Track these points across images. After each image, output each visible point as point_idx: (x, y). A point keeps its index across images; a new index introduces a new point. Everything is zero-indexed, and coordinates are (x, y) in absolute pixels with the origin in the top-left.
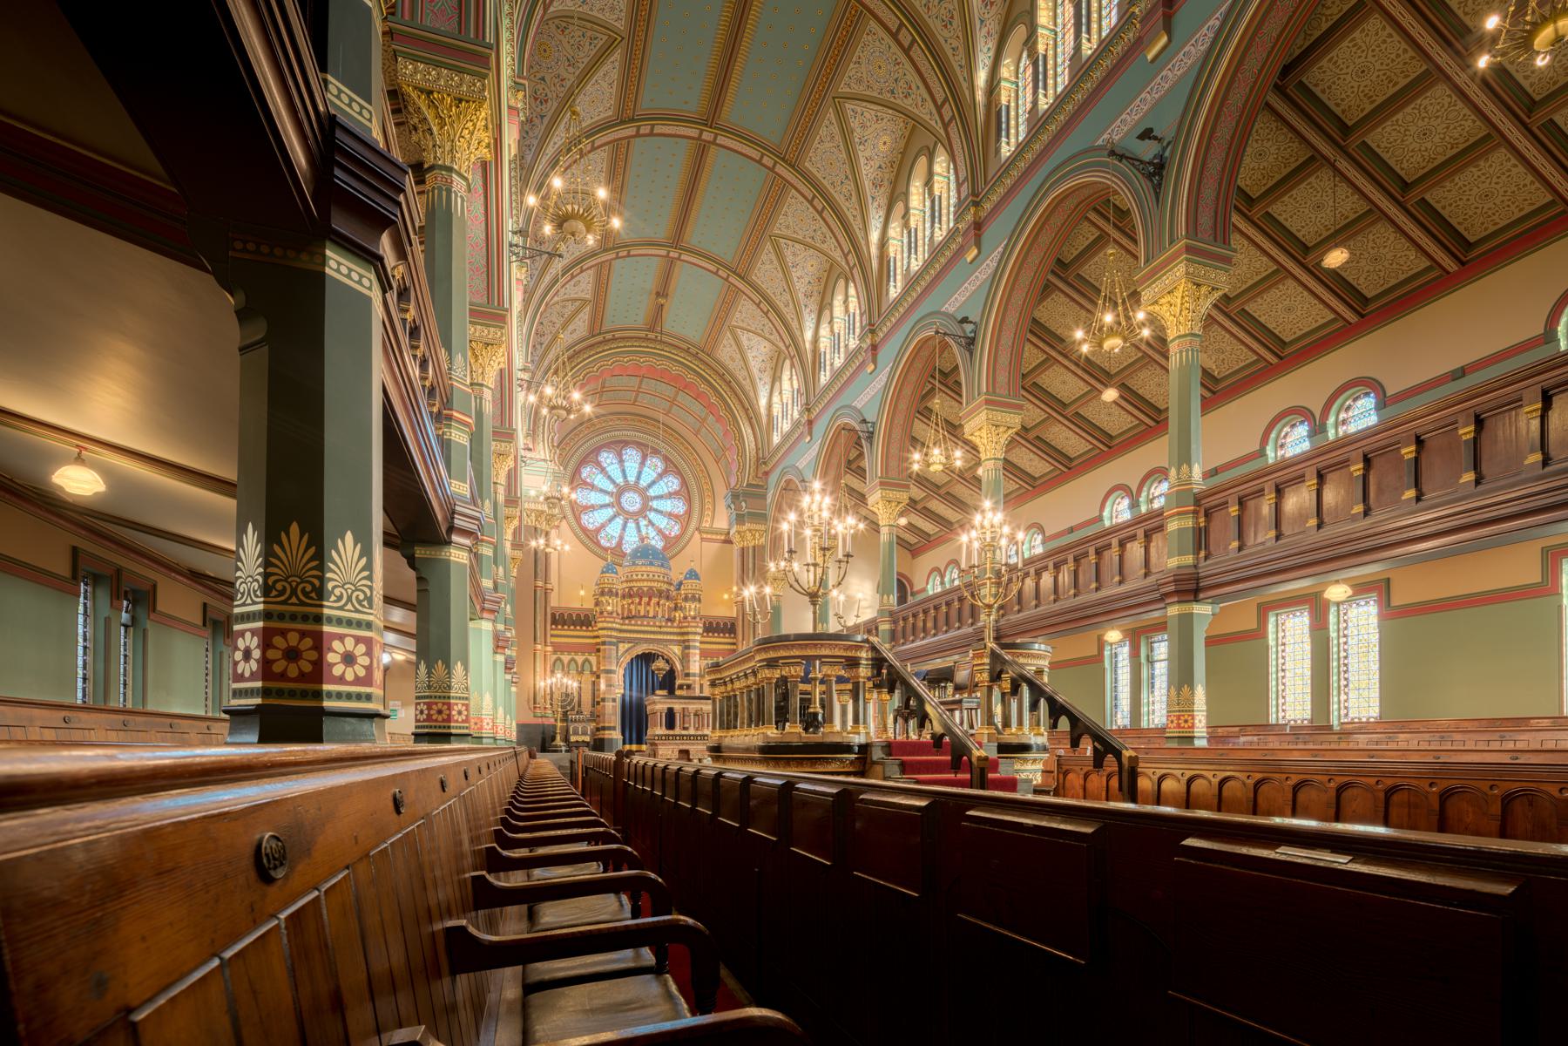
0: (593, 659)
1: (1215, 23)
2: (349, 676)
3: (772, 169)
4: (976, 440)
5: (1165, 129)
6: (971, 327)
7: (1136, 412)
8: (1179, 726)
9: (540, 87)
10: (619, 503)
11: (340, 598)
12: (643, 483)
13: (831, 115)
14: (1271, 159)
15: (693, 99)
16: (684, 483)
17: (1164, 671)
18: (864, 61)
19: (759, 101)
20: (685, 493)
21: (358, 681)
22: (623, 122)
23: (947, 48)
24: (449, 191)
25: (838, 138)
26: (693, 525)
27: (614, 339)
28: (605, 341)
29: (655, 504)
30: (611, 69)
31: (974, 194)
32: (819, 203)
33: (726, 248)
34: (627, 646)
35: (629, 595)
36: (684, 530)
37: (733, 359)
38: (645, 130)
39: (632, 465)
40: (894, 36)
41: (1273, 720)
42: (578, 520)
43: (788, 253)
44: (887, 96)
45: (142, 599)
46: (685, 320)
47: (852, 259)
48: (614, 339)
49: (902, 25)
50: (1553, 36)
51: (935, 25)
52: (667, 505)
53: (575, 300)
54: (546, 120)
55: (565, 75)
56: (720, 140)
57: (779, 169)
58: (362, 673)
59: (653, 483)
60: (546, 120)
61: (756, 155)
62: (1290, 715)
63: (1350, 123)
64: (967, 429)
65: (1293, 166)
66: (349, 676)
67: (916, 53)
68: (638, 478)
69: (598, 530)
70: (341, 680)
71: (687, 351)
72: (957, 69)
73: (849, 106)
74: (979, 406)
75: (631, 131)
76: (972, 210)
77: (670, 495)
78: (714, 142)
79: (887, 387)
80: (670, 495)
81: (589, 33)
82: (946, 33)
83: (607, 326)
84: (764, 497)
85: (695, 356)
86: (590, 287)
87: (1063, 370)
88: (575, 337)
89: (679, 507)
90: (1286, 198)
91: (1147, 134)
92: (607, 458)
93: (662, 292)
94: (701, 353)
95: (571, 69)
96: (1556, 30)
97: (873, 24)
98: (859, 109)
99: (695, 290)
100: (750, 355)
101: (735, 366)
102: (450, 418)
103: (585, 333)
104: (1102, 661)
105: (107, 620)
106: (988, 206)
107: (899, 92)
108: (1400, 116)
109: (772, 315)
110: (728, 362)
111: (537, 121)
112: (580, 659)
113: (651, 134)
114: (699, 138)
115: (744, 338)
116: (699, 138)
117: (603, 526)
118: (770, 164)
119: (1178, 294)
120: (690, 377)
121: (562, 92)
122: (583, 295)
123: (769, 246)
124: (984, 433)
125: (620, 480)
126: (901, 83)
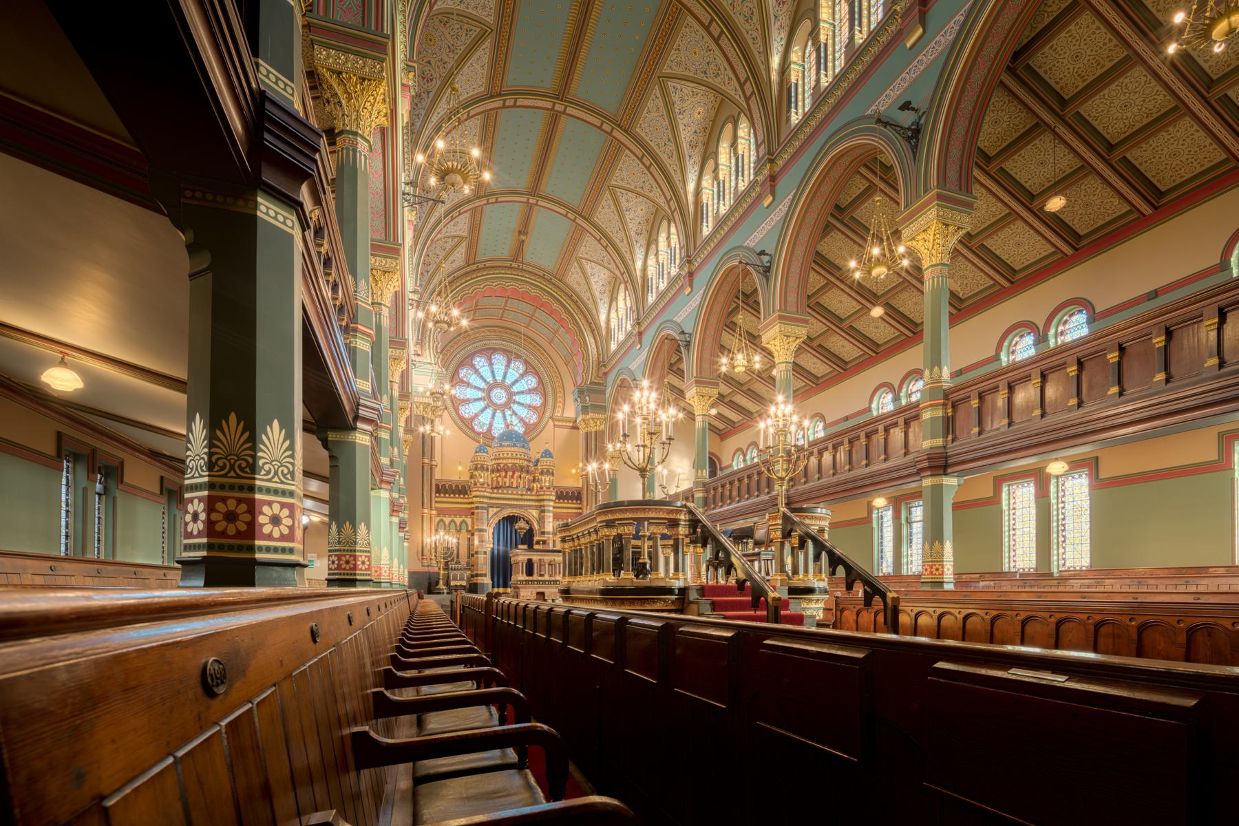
0: (469, 520)
1: (960, 18)
2: (276, 534)
3: (610, 134)
4: (772, 348)
5: (921, 101)
6: (767, 258)
7: (898, 326)
9: (427, 68)
10: (489, 397)
11: (268, 472)
12: (508, 381)
13: (657, 91)
14: (1004, 126)
15: (547, 78)
16: (541, 381)
17: (920, 530)
18: (682, 48)
19: (600, 80)
21: (283, 538)
22: (492, 97)
23: (748, 38)
24: (355, 151)
25: (662, 109)
26: (548, 414)
27: (486, 268)
28: (478, 270)
29: (517, 398)
30: (483, 55)
31: (770, 153)
32: (647, 160)
33: (574, 196)
34: (496, 510)
35: (497, 470)
36: (540, 418)
37: (579, 284)
38: (509, 103)
39: (499, 367)
40: (707, 28)
41: (1006, 569)
42: (457, 410)
43: (623, 200)
44: (701, 76)
45: (112, 473)
46: (541, 253)
47: (673, 205)
48: (486, 268)
49: (712, 19)
50: (1227, 29)
51: (739, 20)
52: (527, 399)
53: (454, 237)
54: (431, 95)
55: (447, 59)
56: (569, 111)
57: (615, 133)
58: (286, 531)
59: (516, 381)
60: (431, 95)
61: (598, 123)
62: (1019, 565)
63: (1067, 98)
64: (764, 339)
65: (1022, 131)
66: (276, 534)
67: (724, 42)
68: (504, 377)
69: (473, 419)
71: (543, 277)
72: (757, 55)
73: (671, 84)
74: (773, 321)
75: (499, 104)
76: (768, 166)
78: (564, 112)
79: (701, 305)
81: (465, 26)
82: (747, 26)
83: (480, 257)
85: (550, 281)
86: (466, 227)
87: (840, 292)
88: (455, 266)
89: (537, 400)
90: (1016, 157)
91: (906, 106)
92: (479, 362)
93: (523, 231)
94: (554, 279)
95: (451, 55)
96: (1230, 24)
97: (690, 19)
98: (679, 86)
99: (549, 229)
100: (592, 280)
101: (580, 289)
102: (355, 330)
103: (463, 263)
104: (871, 522)
105: (85, 490)
106: (781, 163)
107: (710, 73)
108: (1106, 91)
109: (610, 248)
110: (575, 286)
111: (424, 96)
113: (515, 106)
114: (552, 109)
115: (588, 267)
116: (552, 109)
117: (476, 415)
118: (609, 129)
119: (931, 232)
120: (545, 298)
121: (444, 72)
122: (460, 233)
123: (607, 194)
124: (777, 342)
125: (490, 379)
126: (712, 66)
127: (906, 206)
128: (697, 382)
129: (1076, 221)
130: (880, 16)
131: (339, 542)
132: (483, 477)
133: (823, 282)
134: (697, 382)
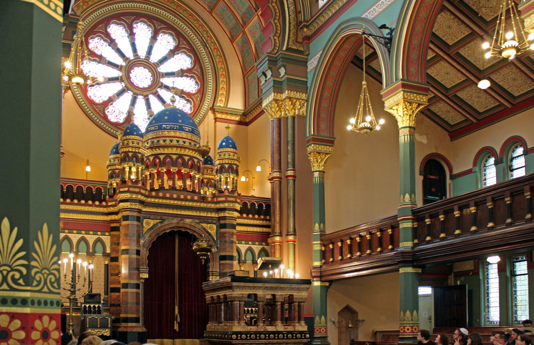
0: (107, 239)
4: (393, 112)
6: (388, 31)
7: (498, 97)
8: (412, 332)
10: (129, 78)
11: (39, 282)
12: (155, 58)
20: (197, 72)
26: (207, 103)
36: (197, 109)
41: (483, 325)
64: (387, 104)
68: (149, 52)
70: (52, 317)
74: (396, 89)
77: (182, 73)
80: (182, 73)
84: (305, 63)
87: (447, 65)
89: (189, 85)
92: (116, 31)
112: (91, 238)
117: (110, 100)
124: (400, 108)
125: (129, 54)
127: (386, 86)
128: (403, 86)
129: (475, 104)
130: (168, 231)
131: (412, 320)
132: (133, 172)
133: (467, 32)
134: (403, 86)
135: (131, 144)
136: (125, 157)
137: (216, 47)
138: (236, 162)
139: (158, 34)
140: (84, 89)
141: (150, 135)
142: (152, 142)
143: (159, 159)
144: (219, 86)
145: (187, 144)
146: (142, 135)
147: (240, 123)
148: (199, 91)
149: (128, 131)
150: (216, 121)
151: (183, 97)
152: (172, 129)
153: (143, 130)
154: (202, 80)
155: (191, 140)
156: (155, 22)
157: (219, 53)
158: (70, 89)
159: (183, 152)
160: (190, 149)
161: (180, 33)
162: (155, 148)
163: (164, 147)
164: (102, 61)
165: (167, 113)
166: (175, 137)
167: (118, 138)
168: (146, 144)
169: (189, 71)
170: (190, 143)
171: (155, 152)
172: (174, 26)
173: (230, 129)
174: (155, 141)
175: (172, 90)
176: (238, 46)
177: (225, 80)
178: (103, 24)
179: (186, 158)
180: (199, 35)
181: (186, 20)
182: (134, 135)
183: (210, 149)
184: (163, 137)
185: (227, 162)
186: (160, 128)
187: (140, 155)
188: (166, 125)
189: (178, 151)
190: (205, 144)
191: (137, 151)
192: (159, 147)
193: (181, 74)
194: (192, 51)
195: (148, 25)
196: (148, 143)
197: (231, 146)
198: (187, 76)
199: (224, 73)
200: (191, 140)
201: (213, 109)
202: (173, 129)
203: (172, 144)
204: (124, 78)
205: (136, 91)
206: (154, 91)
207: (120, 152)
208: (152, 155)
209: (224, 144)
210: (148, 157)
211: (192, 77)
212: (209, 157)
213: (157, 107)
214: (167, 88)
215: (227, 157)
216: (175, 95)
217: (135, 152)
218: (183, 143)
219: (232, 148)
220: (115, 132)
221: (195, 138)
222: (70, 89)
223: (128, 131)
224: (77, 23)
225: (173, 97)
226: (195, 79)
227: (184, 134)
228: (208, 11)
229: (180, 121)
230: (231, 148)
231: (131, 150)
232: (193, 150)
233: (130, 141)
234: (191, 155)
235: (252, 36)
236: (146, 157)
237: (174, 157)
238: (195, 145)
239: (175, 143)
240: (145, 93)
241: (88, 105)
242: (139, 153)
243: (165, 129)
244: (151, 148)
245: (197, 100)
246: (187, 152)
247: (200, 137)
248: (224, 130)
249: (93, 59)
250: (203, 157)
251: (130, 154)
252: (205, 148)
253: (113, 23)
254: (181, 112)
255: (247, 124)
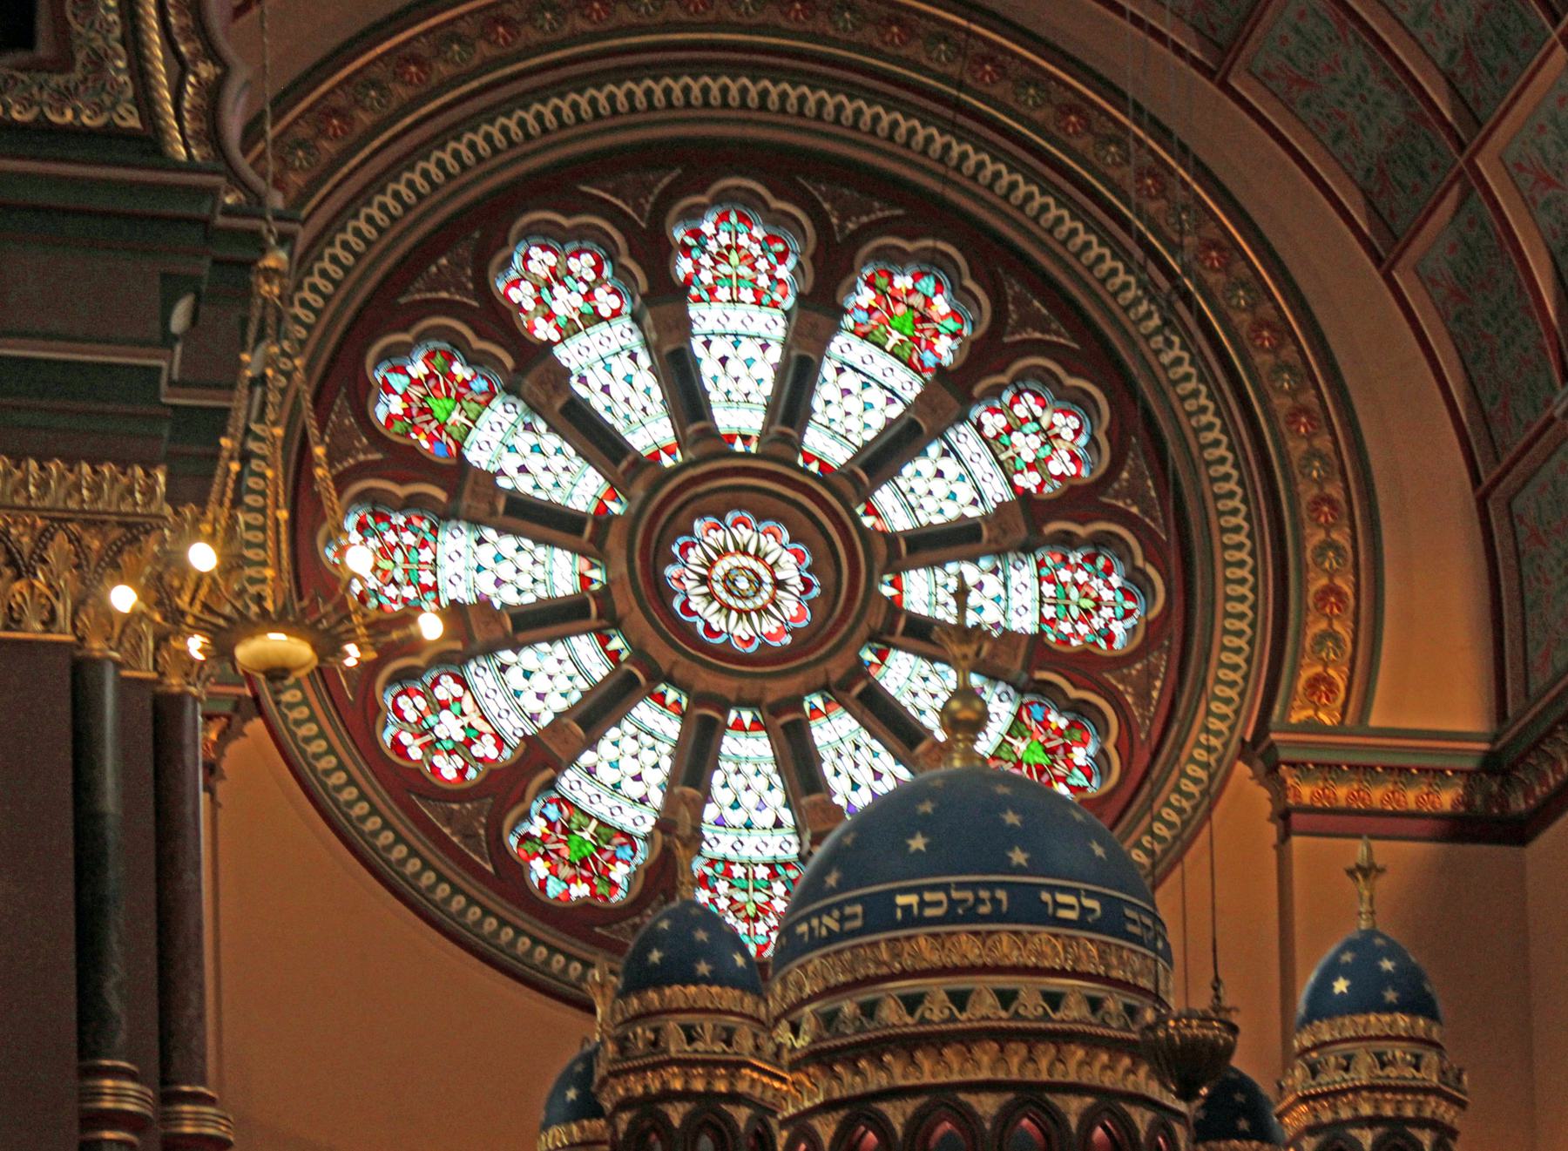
10: (659, 593)
26: (1220, 714)
92: (560, 291)
135: (676, 1045)
136: (644, 1136)
137: (1266, 310)
138: (1447, 1113)
139: (850, 269)
140: (356, 710)
141: (812, 972)
142: (829, 1020)
143: (882, 1126)
144: (1303, 585)
145: (1074, 1012)
146: (756, 977)
147: (1459, 828)
148: (1151, 636)
149: (655, 956)
150: (1285, 835)
151: (1044, 690)
152: (957, 914)
153: (760, 937)
154: (1175, 559)
155: (1107, 980)
156: (818, 191)
157: (1289, 352)
158: (261, 712)
159: (1043, 1069)
160: (1092, 1042)
161: (999, 239)
162: (850, 1054)
163: (908, 1044)
164: (466, 502)
165: (927, 807)
166: (984, 969)
167: (592, 1011)
168: (784, 1035)
169: (1077, 499)
170: (1095, 1004)
171: (850, 1084)
172: (953, 196)
173: (1382, 883)
174: (848, 1008)
175: (956, 650)
176: (1429, 282)
177: (1341, 537)
178: (464, 251)
179: (1073, 1108)
180: (1125, 224)
181: (1004, 131)
182: (697, 981)
183: (1233, 1029)
184: (904, 974)
185: (1366, 1110)
186: (880, 915)
187: (742, 1115)
188: (918, 890)
189: (1015, 1067)
190: (1202, 1002)
191: (721, 1087)
192: (875, 1049)
193: (1022, 534)
194: (1096, 365)
195: (775, 220)
196: (795, 1029)
197: (1390, 996)
198: (1067, 541)
199: (1334, 491)
200: (1107, 980)
201: (1259, 750)
202: (972, 916)
203: (965, 1019)
204: (624, 603)
205: (707, 681)
206: (836, 669)
207: (608, 1106)
208: (829, 1106)
209: (1341, 986)
210: (800, 1125)
211: (1100, 542)
212: (1243, 1084)
213: (858, 768)
214: (922, 636)
215: (1362, 1074)
216: (975, 680)
217: (710, 1098)
218: (1084, 1011)
219: (1403, 1006)
220: (576, 968)
221: (1130, 963)
222: (261, 712)
223: (655, 956)
224: (247, 265)
225: (964, 693)
226: (1125, 554)
227: (1043, 944)
228: (1195, 63)
229: (1018, 857)
230: (1390, 1009)
231: (677, 1085)
232: (1116, 1046)
233: (672, 1025)
234: (1108, 1080)
235: (1529, 203)
236: (784, 1124)
237: (987, 1105)
238: (1131, 1011)
239: (985, 1009)
240: (776, 690)
241: (381, 798)
242: (735, 1098)
243: (912, 919)
244: (820, 1058)
245: (1143, 697)
246: (1074, 1065)
247: (1166, 954)
248: (1363, 888)
249: (401, 491)
250: (1186, 1094)
251: (676, 1114)
252: (1196, 1030)
253: (527, 234)
254: (1032, 793)
255: (1518, 832)
